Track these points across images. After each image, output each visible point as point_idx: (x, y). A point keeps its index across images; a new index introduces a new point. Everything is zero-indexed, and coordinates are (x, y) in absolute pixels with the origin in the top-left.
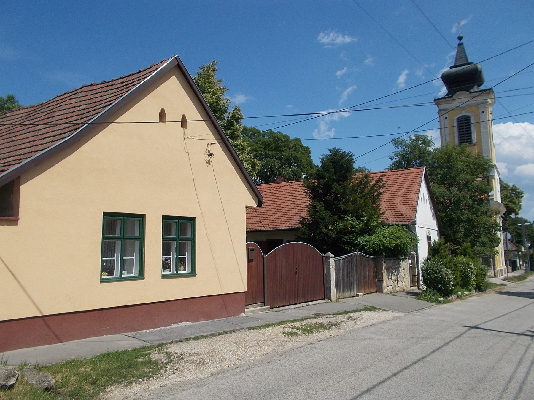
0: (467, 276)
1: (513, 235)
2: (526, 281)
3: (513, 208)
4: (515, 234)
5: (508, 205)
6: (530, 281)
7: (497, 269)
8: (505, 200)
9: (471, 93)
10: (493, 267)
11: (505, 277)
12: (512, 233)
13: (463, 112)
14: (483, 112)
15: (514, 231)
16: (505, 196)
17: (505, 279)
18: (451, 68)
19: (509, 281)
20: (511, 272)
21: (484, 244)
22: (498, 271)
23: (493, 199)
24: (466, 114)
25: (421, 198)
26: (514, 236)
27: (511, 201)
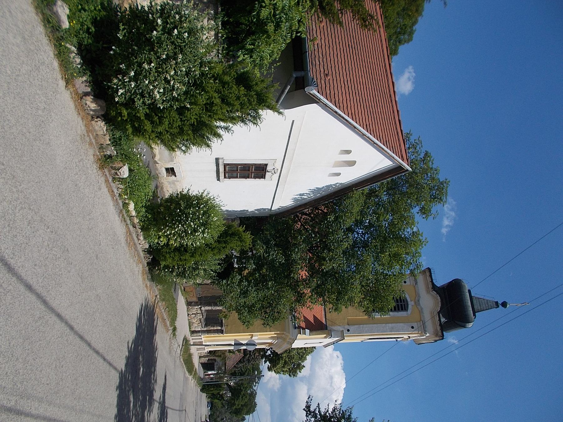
0: (177, 220)
1: (242, 368)
2: (185, 373)
3: (278, 365)
4: (243, 370)
5: (281, 359)
6: (186, 379)
7: (202, 336)
8: (288, 356)
9: (439, 313)
10: (206, 329)
11: (189, 341)
12: (244, 368)
13: (413, 303)
14: (413, 327)
15: (247, 370)
16: (293, 356)
17: (186, 340)
18: (469, 291)
19: (183, 345)
20: (201, 361)
21: (245, 293)
22: (200, 337)
23: (301, 334)
24: (410, 307)
25: (338, 174)
26: (241, 369)
27: (286, 363)
